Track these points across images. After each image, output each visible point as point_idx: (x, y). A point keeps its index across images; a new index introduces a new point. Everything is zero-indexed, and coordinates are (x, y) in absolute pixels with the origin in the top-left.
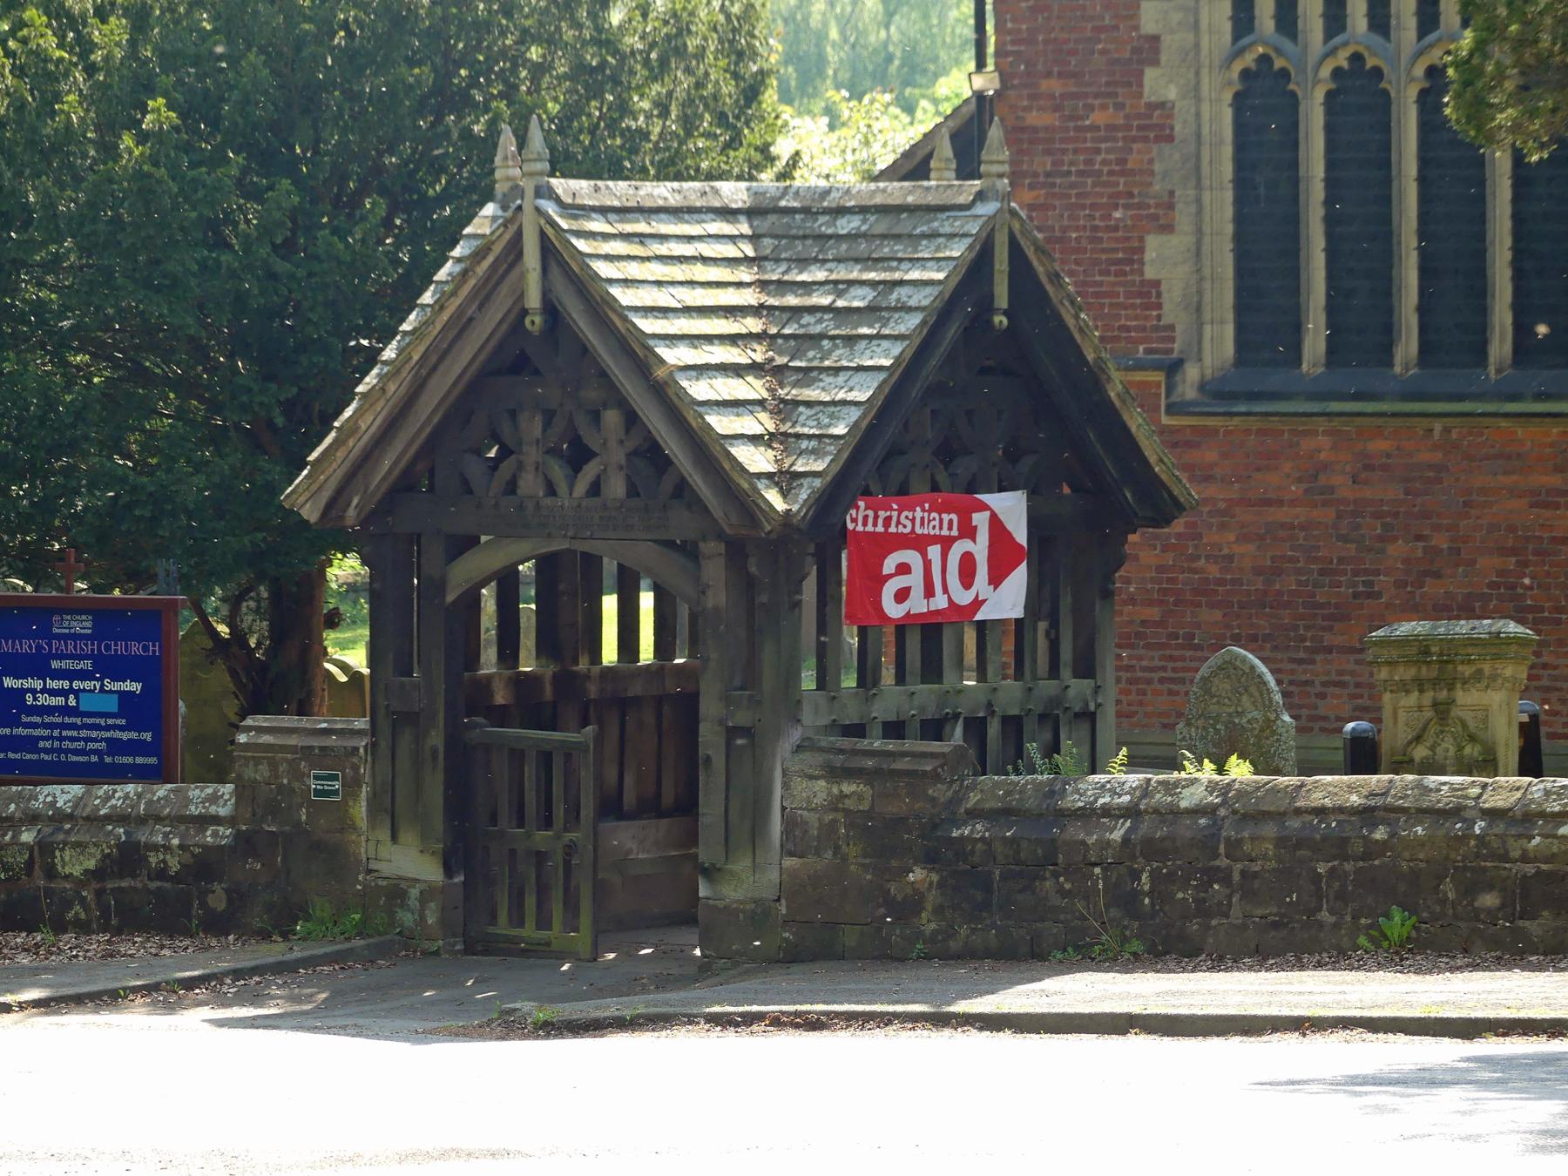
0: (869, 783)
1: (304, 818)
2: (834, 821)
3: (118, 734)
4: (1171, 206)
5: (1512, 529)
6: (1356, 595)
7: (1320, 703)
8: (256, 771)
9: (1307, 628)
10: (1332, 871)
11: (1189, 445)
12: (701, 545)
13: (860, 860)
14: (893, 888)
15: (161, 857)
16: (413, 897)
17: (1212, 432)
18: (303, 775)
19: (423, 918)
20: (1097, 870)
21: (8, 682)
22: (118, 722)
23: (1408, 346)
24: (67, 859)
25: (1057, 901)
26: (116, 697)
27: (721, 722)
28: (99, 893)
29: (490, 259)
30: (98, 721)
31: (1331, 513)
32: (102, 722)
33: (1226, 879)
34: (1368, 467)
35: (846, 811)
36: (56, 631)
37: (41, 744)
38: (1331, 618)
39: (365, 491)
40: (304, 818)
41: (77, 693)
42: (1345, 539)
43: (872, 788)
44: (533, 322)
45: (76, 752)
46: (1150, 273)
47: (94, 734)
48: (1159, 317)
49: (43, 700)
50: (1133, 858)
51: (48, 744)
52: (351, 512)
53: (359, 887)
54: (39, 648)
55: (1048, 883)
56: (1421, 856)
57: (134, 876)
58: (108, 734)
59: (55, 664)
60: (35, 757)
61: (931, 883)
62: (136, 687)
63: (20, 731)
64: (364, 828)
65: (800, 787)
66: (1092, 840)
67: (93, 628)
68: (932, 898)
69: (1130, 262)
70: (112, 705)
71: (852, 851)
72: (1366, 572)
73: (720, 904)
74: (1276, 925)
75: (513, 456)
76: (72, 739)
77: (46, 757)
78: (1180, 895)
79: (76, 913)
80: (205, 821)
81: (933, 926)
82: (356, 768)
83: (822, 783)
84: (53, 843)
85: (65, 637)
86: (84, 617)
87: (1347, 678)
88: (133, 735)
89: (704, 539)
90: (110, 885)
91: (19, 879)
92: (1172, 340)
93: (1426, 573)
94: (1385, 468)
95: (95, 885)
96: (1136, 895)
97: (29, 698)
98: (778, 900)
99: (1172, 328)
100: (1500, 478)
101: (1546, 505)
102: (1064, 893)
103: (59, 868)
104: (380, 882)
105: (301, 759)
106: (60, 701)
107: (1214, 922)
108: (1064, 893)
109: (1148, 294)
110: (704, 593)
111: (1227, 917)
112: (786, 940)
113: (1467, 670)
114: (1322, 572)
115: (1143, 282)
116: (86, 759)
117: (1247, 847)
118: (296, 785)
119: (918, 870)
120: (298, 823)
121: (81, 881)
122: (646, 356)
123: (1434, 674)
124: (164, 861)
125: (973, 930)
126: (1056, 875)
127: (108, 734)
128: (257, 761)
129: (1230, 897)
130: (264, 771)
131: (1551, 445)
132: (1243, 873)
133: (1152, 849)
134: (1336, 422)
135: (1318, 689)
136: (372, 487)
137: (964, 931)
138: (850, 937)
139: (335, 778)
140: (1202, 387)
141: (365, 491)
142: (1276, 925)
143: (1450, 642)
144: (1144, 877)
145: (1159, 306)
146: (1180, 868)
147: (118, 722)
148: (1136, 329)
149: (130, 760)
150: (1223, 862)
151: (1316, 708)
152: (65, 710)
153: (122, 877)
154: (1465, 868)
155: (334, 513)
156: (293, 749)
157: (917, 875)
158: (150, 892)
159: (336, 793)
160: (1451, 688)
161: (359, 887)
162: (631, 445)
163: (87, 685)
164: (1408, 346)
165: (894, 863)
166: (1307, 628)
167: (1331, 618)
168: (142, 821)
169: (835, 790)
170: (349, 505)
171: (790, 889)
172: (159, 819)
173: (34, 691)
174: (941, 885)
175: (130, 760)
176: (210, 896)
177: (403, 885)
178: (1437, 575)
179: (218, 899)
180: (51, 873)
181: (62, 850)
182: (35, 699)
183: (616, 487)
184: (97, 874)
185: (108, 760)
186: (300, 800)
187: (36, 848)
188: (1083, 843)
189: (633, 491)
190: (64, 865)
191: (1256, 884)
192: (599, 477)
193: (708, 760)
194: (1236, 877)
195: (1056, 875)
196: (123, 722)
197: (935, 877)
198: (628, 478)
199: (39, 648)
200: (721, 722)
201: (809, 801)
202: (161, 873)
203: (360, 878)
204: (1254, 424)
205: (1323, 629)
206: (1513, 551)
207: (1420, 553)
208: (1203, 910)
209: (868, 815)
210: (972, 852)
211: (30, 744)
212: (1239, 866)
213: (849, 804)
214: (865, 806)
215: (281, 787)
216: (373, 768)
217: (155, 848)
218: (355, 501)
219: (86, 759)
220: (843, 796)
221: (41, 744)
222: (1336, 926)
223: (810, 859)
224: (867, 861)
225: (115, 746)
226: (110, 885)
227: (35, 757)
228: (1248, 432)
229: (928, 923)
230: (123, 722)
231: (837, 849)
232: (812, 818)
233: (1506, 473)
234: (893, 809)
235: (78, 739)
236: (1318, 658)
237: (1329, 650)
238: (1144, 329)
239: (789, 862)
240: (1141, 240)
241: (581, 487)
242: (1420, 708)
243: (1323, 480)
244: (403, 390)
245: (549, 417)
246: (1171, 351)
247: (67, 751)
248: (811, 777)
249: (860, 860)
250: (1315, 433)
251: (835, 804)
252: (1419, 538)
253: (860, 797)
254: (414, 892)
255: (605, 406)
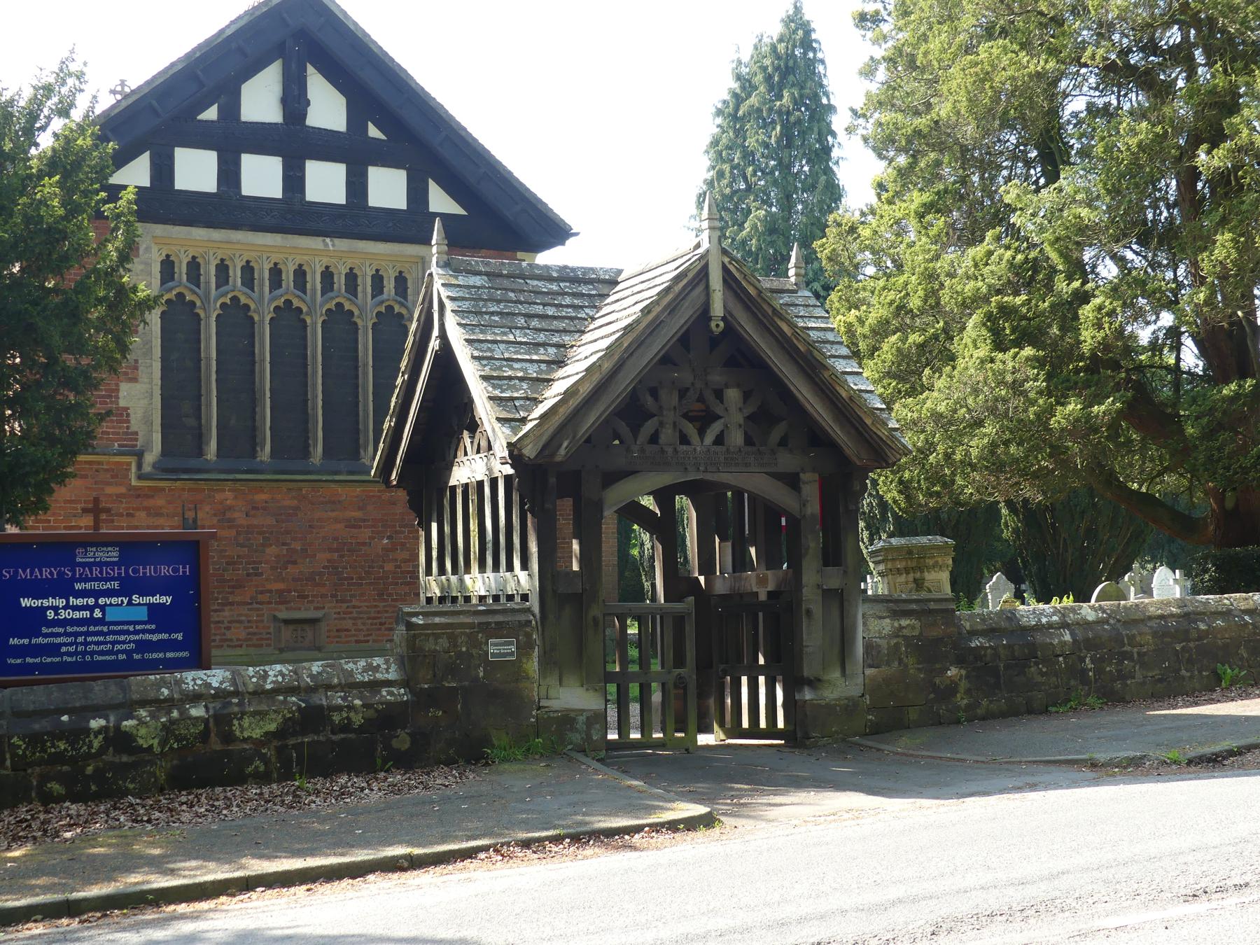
0: (917, 618)
1: (481, 674)
2: (897, 645)
3: (148, 637)
4: (136, 368)
5: (336, 539)
6: (248, 575)
7: (227, 632)
8: (436, 644)
9: (218, 593)
10: (1183, 648)
11: (147, 496)
12: (802, 475)
13: (916, 666)
14: (937, 681)
15: (345, 715)
16: (580, 721)
17: (163, 489)
18: (481, 643)
19: (589, 736)
20: (1061, 659)
21: (25, 602)
22: (148, 627)
23: (265, 453)
24: (246, 725)
25: (1039, 679)
26: (145, 608)
27: (818, 586)
28: (280, 751)
29: (685, 281)
30: (125, 628)
31: (233, 532)
32: (131, 628)
33: (1131, 658)
34: (254, 508)
35: (905, 638)
36: (79, 560)
37: (64, 649)
38: (233, 587)
39: (574, 437)
40: (481, 674)
41: (103, 608)
42: (242, 546)
43: (920, 621)
44: (717, 326)
45: (102, 653)
46: (122, 403)
47: (122, 638)
48: (128, 428)
49: (64, 614)
50: (1080, 650)
51: (72, 649)
52: (562, 451)
53: (533, 720)
54: (60, 574)
55: (1032, 669)
56: (1227, 636)
57: (317, 733)
58: (137, 637)
59: (78, 586)
60: (58, 659)
61: (961, 676)
62: (167, 600)
63: (40, 640)
64: (537, 677)
65: (875, 625)
66: (1056, 641)
67: (119, 557)
68: (964, 685)
69: (110, 397)
70: (143, 614)
71: (910, 661)
72: (254, 562)
73: (823, 703)
74: (1160, 681)
75: (656, 418)
76: (98, 643)
77: (69, 659)
78: (1108, 669)
79: (257, 767)
80: (375, 685)
81: (965, 701)
82: (528, 636)
83: (888, 621)
84: (230, 714)
85: (90, 565)
86: (110, 549)
87: (243, 618)
88: (165, 636)
89: (803, 470)
90: (292, 742)
91: (193, 746)
92: (136, 440)
93: (289, 562)
94: (265, 509)
95: (276, 743)
96: (1084, 671)
97: (51, 615)
98: (863, 695)
99: (136, 433)
100: (330, 513)
101: (354, 527)
102: (1043, 674)
103: (238, 733)
104: (552, 715)
105: (478, 632)
106: (86, 614)
107: (1129, 682)
108: (1043, 674)
109: (121, 415)
110: (804, 505)
111: (1134, 678)
112: (871, 720)
113: (931, 562)
114: (227, 563)
115: (118, 409)
116: (113, 657)
117: (1138, 639)
118: (474, 652)
119: (953, 669)
120: (477, 678)
121: (261, 741)
122: (811, 353)
123: (914, 564)
124: (348, 718)
125: (991, 702)
126: (1037, 664)
127: (137, 637)
128: (437, 636)
129: (1134, 667)
130: (444, 643)
131: (357, 497)
132: (1139, 653)
133: (1090, 644)
134: (238, 485)
135: (226, 624)
136: (580, 434)
137: (985, 702)
138: (913, 715)
139: (511, 643)
140: (154, 466)
141: (574, 437)
142: (1160, 681)
143: (923, 548)
144: (1087, 660)
145: (128, 421)
146: (1106, 653)
147: (148, 627)
148: (113, 433)
149: (161, 655)
150: (1127, 648)
151: (224, 634)
152: (92, 621)
153: (304, 734)
154: (1250, 641)
155: (547, 452)
156: (471, 626)
157: (952, 672)
158: (333, 742)
159: (512, 654)
160: (922, 572)
161: (533, 720)
162: (748, 411)
163: (114, 600)
164: (265, 453)
165: (938, 666)
166: (218, 593)
167: (233, 587)
168: (311, 690)
169: (896, 624)
170: (560, 445)
171: (872, 688)
172: (329, 687)
173: (56, 609)
174: (967, 677)
175: (161, 655)
176: (395, 740)
177: (572, 715)
178: (295, 563)
179: (402, 741)
180: (228, 738)
181: (241, 718)
182: (57, 614)
183: (736, 438)
184: (279, 734)
185: (137, 657)
186: (478, 662)
187: (211, 720)
188: (1051, 644)
189: (749, 441)
190: (242, 729)
191: (1146, 658)
192: (722, 432)
193: (809, 612)
194: (1136, 655)
195: (1037, 664)
196: (153, 627)
197: (963, 672)
198: (746, 433)
199: (60, 574)
200: (818, 586)
201: (880, 632)
202: (346, 727)
203: (534, 713)
204: (189, 484)
205: (229, 593)
206: (337, 550)
207: (285, 552)
208: (1122, 676)
209: (918, 638)
210: (985, 655)
211: (54, 650)
212: (1135, 650)
213: (906, 632)
214: (916, 633)
215: (460, 655)
216: (543, 634)
217: (339, 709)
218: (565, 444)
219: (113, 657)
220: (901, 628)
221: (64, 649)
222: (1191, 677)
223: (884, 668)
224: (920, 666)
225: (143, 646)
226: (292, 742)
227: (58, 659)
228: (183, 490)
229: (962, 700)
230: (153, 627)
231: (900, 661)
232: (883, 643)
233: (333, 511)
234: (934, 633)
235: (105, 643)
236: (226, 608)
237: (232, 604)
238: (118, 434)
239: (869, 672)
240: (117, 385)
241: (709, 438)
242: (907, 583)
243: (228, 515)
244: (611, 366)
245: (683, 393)
246: (136, 446)
247: (92, 653)
248: (881, 618)
249: (916, 666)
250: (224, 491)
251: (897, 633)
252: (284, 544)
253: (913, 628)
254: (582, 719)
255: (727, 386)
